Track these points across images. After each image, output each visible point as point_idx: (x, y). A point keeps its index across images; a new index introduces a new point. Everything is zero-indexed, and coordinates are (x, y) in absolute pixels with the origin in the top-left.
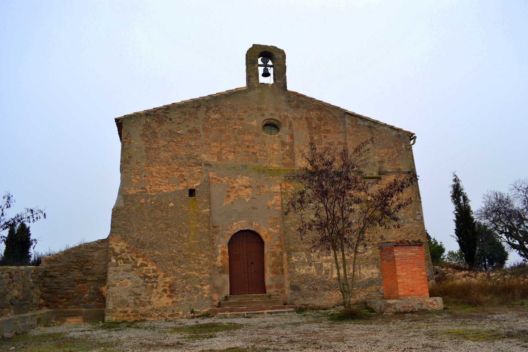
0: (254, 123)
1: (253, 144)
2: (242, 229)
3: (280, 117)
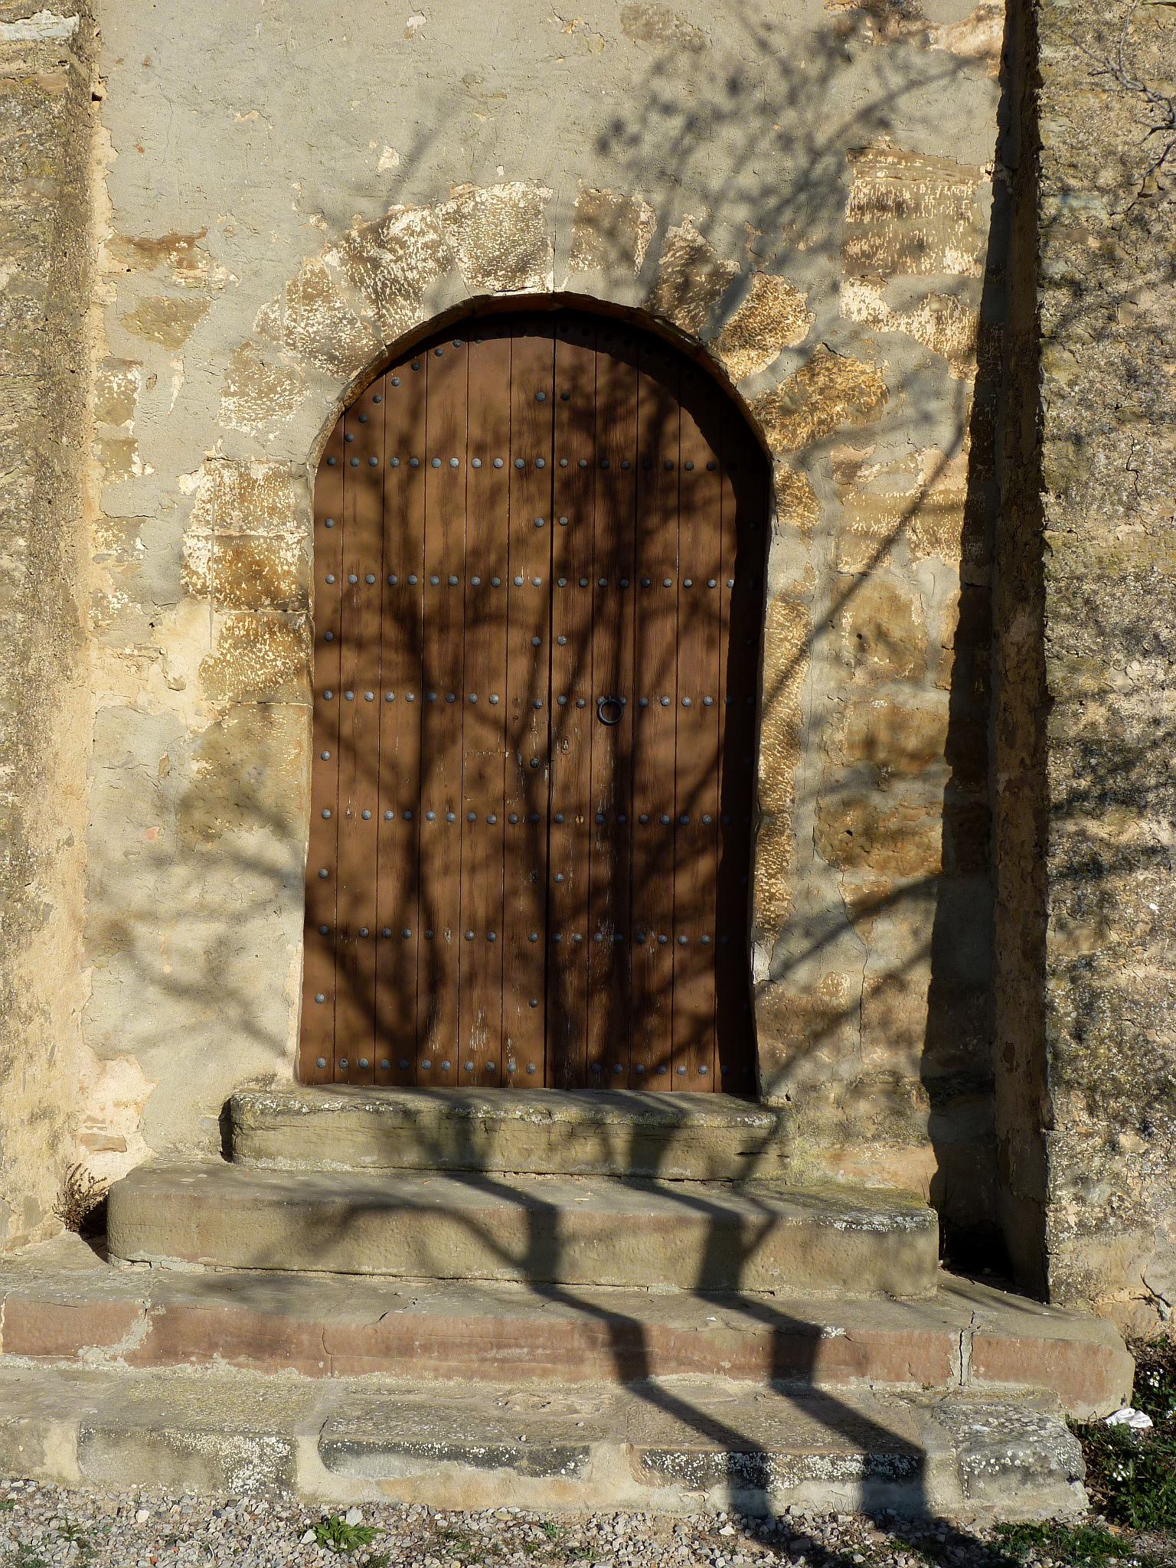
2: (493, 287)
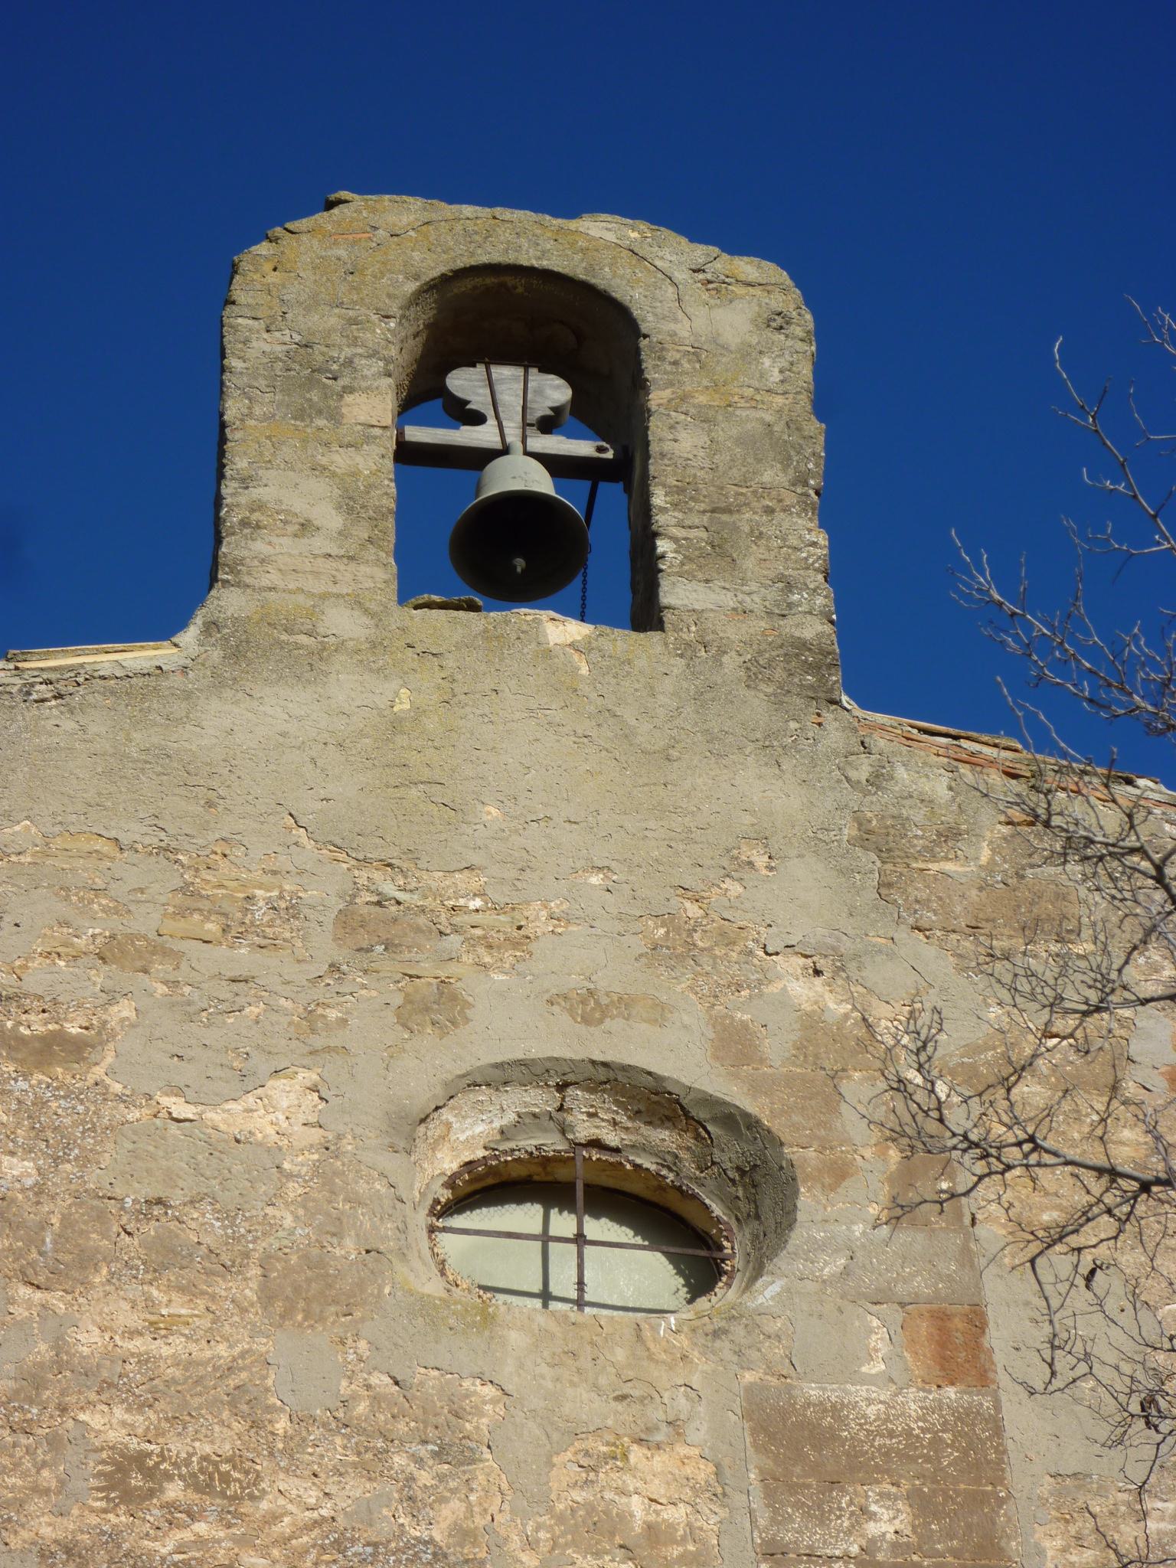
0: (278, 1111)
1: (220, 1439)
3: (735, 1044)
